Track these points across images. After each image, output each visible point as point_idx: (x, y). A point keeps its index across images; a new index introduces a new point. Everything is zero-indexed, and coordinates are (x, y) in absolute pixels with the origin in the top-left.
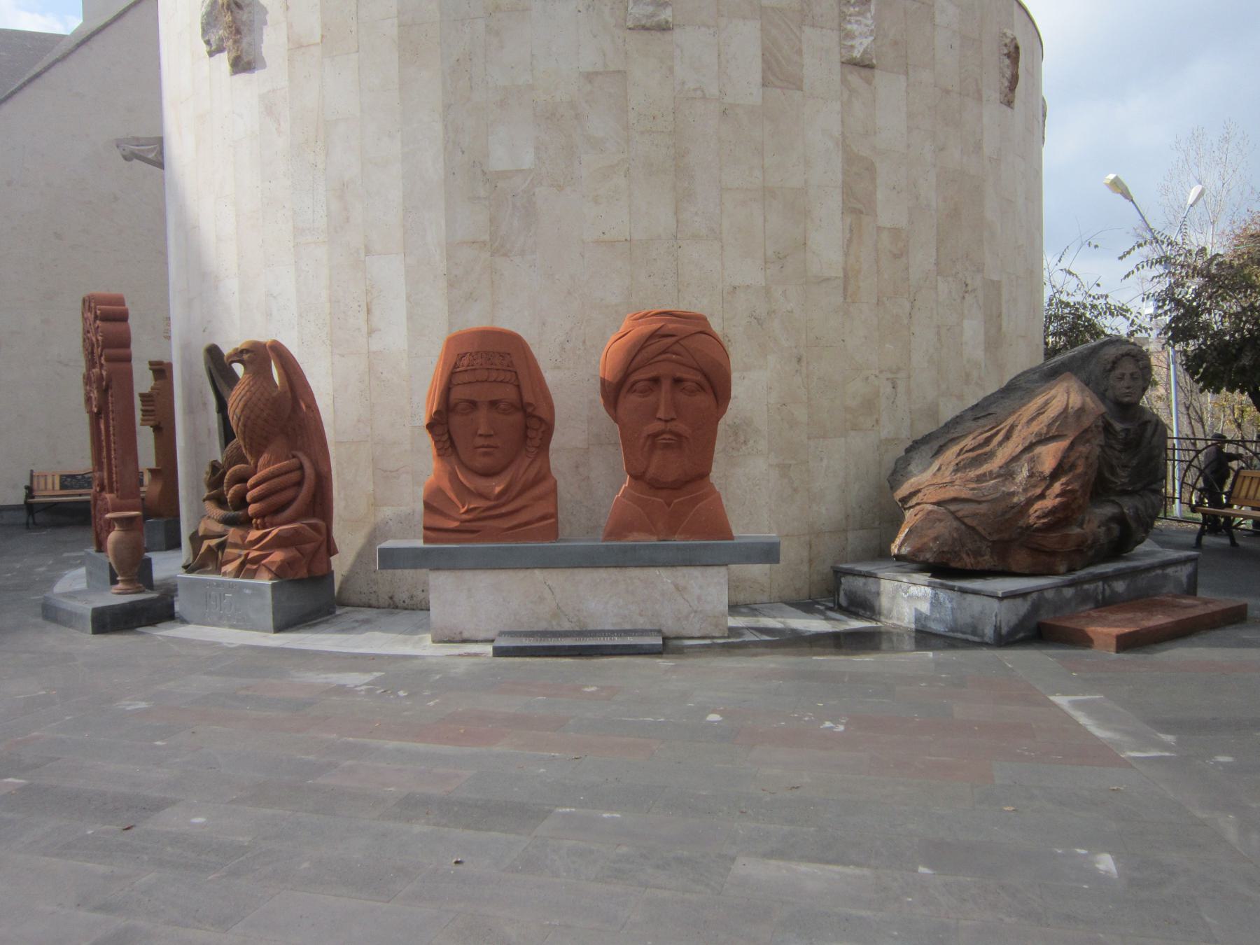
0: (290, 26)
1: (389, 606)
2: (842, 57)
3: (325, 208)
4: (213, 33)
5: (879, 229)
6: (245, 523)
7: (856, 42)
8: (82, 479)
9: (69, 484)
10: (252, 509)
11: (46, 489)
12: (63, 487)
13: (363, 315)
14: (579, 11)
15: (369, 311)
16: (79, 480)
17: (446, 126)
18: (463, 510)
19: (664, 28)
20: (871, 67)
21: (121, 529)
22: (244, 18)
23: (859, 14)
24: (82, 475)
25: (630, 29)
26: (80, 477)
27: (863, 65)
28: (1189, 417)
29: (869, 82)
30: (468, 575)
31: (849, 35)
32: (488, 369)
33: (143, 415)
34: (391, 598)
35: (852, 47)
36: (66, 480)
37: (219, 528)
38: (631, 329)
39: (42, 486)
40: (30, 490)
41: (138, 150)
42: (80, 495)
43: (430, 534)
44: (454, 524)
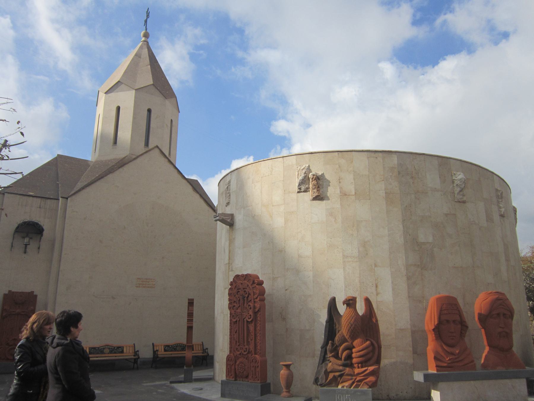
0: (341, 188)
1: (387, 399)
2: (499, 214)
3: (357, 249)
4: (303, 186)
6: (351, 366)
8: (98, 349)
9: (92, 352)
12: (165, 350)
13: (374, 288)
14: (442, 195)
15: (376, 287)
16: (170, 348)
17: (403, 226)
18: (447, 359)
19: (464, 202)
21: (287, 369)
22: (321, 183)
24: (98, 348)
25: (456, 202)
26: (97, 349)
31: (500, 208)
32: (452, 309)
34: (388, 396)
37: (341, 368)
38: (488, 297)
41: (225, 218)
42: (97, 357)
43: (438, 368)
44: (445, 365)
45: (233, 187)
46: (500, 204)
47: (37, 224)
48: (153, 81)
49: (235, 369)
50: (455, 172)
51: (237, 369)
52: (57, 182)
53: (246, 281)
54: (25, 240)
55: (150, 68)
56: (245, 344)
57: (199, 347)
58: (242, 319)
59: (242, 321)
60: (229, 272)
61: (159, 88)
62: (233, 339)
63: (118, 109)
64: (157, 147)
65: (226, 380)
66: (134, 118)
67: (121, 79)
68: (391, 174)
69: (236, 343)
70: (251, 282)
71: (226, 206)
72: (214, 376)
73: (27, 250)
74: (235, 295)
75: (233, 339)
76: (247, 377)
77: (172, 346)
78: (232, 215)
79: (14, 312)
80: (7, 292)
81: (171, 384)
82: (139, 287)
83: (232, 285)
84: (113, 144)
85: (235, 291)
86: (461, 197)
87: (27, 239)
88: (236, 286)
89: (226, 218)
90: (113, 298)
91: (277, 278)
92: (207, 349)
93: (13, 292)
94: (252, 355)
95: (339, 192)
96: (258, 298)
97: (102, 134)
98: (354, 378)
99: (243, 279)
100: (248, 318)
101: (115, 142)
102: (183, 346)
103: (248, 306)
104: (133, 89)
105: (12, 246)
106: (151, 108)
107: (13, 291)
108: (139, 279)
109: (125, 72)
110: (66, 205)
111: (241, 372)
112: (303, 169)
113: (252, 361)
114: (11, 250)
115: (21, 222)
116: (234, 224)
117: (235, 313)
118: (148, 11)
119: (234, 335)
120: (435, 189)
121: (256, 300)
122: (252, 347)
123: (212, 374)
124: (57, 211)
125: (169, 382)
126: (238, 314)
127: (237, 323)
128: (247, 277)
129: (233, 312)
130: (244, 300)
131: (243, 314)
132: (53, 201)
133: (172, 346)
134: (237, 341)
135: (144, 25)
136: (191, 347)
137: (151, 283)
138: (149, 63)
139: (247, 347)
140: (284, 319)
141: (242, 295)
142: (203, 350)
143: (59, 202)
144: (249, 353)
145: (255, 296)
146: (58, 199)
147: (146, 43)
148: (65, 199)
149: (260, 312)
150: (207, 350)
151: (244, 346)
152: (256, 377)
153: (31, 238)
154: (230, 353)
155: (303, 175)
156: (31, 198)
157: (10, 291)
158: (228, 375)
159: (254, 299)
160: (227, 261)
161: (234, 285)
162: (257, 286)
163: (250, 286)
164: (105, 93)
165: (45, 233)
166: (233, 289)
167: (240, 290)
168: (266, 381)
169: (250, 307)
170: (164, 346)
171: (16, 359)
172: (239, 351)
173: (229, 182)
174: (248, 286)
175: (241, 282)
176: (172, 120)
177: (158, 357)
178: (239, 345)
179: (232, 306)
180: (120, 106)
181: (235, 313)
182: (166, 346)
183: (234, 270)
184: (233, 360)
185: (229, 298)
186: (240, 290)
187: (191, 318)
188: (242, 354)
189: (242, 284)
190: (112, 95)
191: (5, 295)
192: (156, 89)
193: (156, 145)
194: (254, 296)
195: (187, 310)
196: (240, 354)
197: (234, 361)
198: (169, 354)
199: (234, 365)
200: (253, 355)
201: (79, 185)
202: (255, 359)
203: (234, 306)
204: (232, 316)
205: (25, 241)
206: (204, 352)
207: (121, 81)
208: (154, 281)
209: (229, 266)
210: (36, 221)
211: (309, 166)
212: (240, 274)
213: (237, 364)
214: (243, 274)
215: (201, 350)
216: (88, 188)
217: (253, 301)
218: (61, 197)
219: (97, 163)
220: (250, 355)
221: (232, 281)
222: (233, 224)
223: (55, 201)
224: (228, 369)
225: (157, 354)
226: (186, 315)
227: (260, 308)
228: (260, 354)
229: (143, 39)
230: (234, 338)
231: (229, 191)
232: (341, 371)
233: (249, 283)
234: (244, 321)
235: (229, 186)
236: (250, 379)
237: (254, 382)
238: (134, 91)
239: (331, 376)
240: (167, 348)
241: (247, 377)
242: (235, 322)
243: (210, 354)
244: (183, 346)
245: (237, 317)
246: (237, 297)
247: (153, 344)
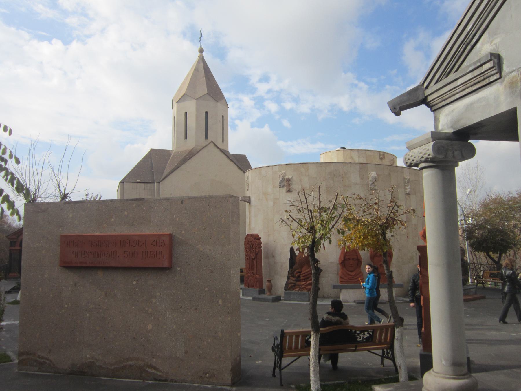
1: (323, 298)
5: (412, 224)
7: (407, 190)
10: (301, 278)
20: (410, 194)
22: (291, 182)
23: (407, 185)
27: (408, 194)
28: (472, 254)
29: (409, 197)
30: (349, 290)
31: (406, 189)
35: (407, 191)
44: (346, 281)
46: (406, 187)
50: (370, 172)
52: (153, 170)
53: (251, 238)
55: (205, 80)
61: (212, 95)
63: (186, 113)
64: (212, 142)
68: (330, 176)
76: (253, 286)
78: (249, 197)
85: (247, 243)
86: (373, 187)
95: (300, 188)
98: (300, 286)
104: (194, 99)
106: (207, 111)
109: (189, 86)
112: (281, 174)
120: (356, 183)
121: (256, 248)
122: (255, 271)
124: (154, 190)
128: (252, 235)
132: (151, 184)
138: (204, 75)
140: (273, 257)
144: (254, 274)
146: (154, 183)
147: (201, 57)
148: (158, 183)
155: (282, 178)
156: (139, 184)
159: (255, 247)
162: (257, 241)
163: (253, 240)
168: (263, 288)
171: (327, 318)
174: (252, 240)
179: (246, 250)
193: (211, 141)
201: (166, 172)
207: (186, 94)
211: (285, 172)
213: (249, 279)
216: (171, 175)
217: (255, 248)
218: (156, 182)
220: (254, 275)
232: (294, 283)
239: (290, 286)
241: (253, 286)
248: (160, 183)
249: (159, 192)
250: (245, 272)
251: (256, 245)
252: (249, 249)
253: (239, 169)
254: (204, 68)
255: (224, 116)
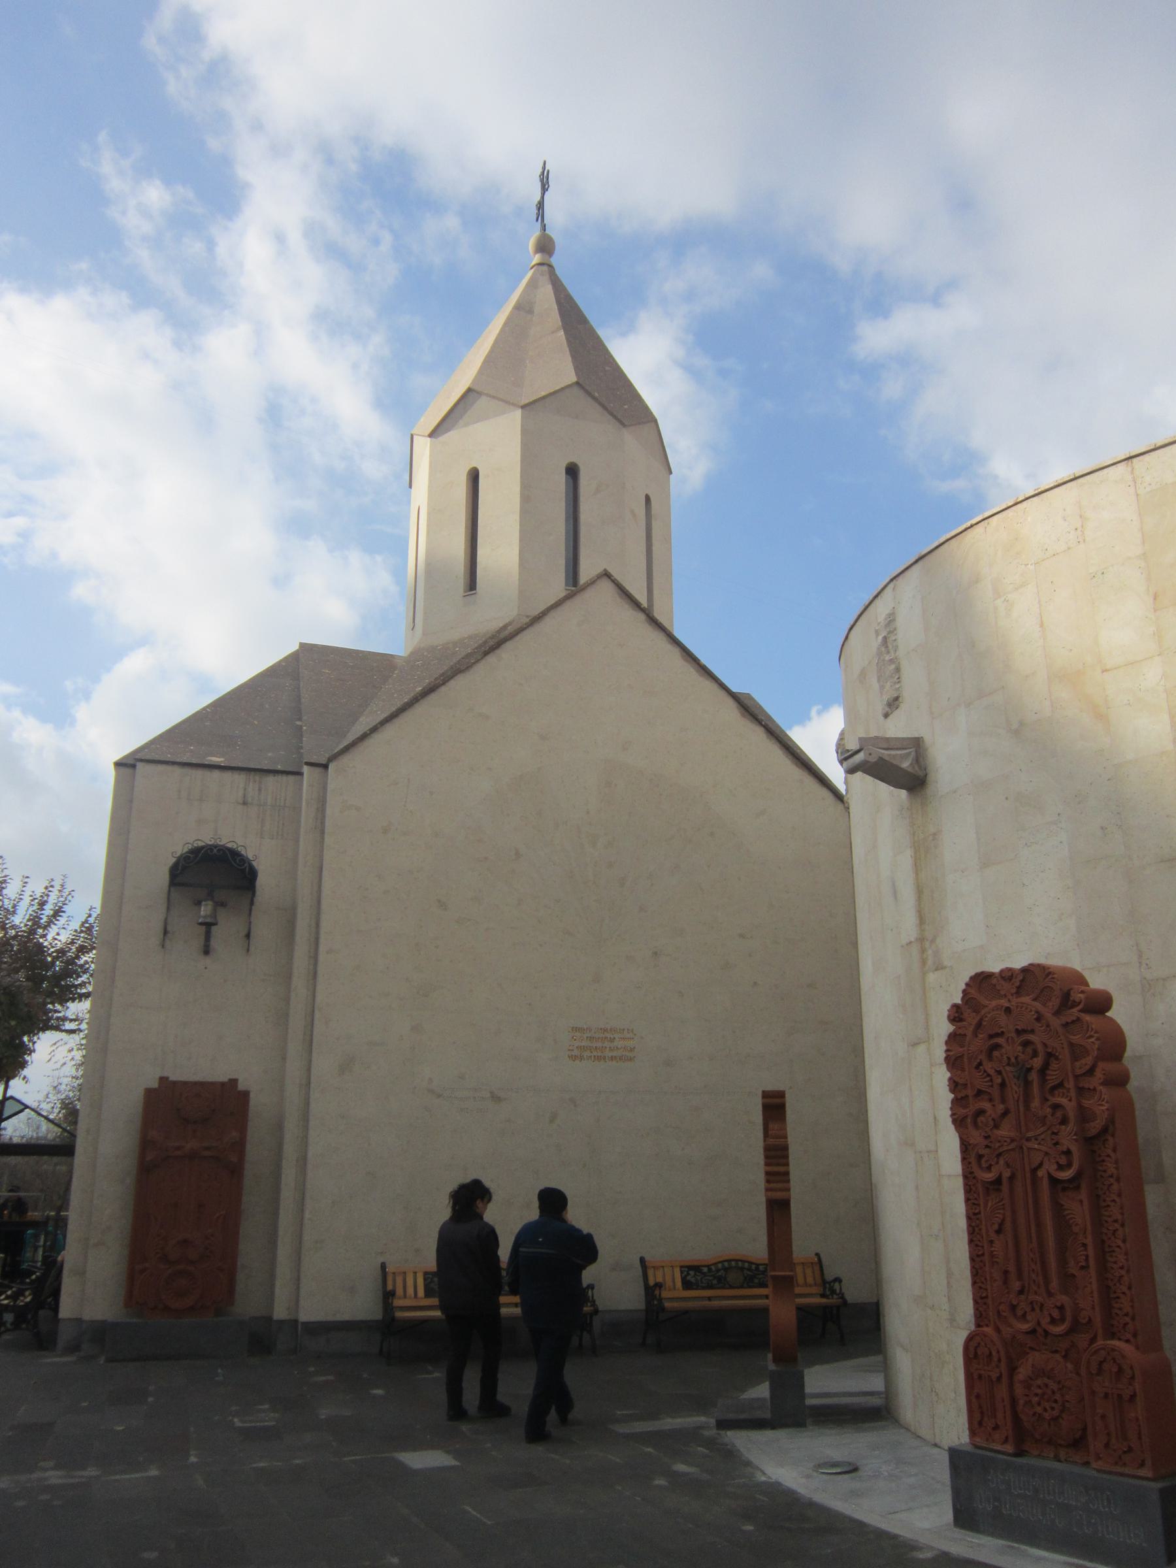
11: (405, 1296)
12: (687, 1285)
16: (704, 1274)
33: (768, 1181)
36: (688, 1274)
39: (399, 1291)
40: (388, 1296)
41: (890, 755)
45: (910, 632)
47: (235, 854)
48: (577, 374)
49: (1013, 1401)
51: (1021, 1402)
52: (298, 723)
53: (1026, 999)
54: (202, 908)
55: (564, 337)
56: (1054, 1284)
57: (809, 1272)
58: (1028, 1175)
59: (1028, 1182)
60: (924, 974)
61: (596, 394)
62: (986, 1258)
63: (474, 477)
64: (606, 575)
65: (970, 1448)
66: (525, 498)
67: (474, 381)
69: (1005, 1282)
70: (1055, 1002)
71: (886, 716)
72: (889, 1393)
73: (214, 943)
74: (980, 1064)
75: (986, 1258)
76: (1078, 1443)
77: (710, 1270)
78: (917, 745)
79: (178, 1148)
80: (155, 1085)
81: (723, 1432)
82: (581, 1058)
83: (961, 1020)
84: (465, 592)
87: (206, 905)
88: (979, 1025)
89: (894, 756)
90: (496, 1099)
91: (1164, 980)
92: (838, 1280)
93: (174, 1083)
94: (1093, 1340)
96: (1099, 1073)
97: (428, 564)
99: (1014, 991)
100: (1055, 1166)
101: (472, 584)
102: (749, 1269)
103: (1049, 1110)
104: (514, 405)
105: (166, 932)
107: (173, 1078)
108: (575, 1029)
110: (324, 788)
111: (1047, 1415)
113: (1100, 1371)
114: (163, 946)
115: (186, 850)
116: (931, 778)
117: (986, 1142)
118: (544, 172)
119: (991, 1242)
123: (876, 1383)
125: (712, 1421)
126: (1005, 1148)
127: (999, 1190)
129: (976, 1137)
130: (1027, 1084)
131: (1029, 1149)
132: (284, 779)
133: (708, 1266)
134: (1012, 1268)
135: (535, 220)
136: (785, 1284)
137: (621, 1042)
138: (561, 324)
139: (1064, 1299)
141: (1013, 1060)
142: (824, 1282)
143: (301, 785)
145: (1083, 1061)
147: (545, 268)
148: (318, 770)
149: (1113, 1136)
150: (837, 1286)
151: (1050, 1294)
152: (1130, 1450)
153: (223, 904)
154: (978, 1325)
156: (216, 774)
157: (163, 1080)
158: (980, 1424)
159: (1076, 1077)
160: (909, 927)
161: (971, 1019)
162: (1087, 1018)
163: (1048, 1015)
164: (431, 435)
165: (261, 881)
166: (968, 1039)
167: (1000, 1040)
169: (1059, 1114)
170: (681, 1267)
172: (1024, 1315)
173: (891, 619)
175: (1004, 1003)
176: (648, 499)
177: (663, 1309)
178: (1021, 1292)
180: (478, 467)
181: (986, 1142)
182: (690, 1268)
183: (946, 963)
184: (999, 1360)
185: (950, 1079)
186: (1000, 1040)
187: (782, 1169)
188: (1039, 1330)
189: (1008, 1010)
190: (452, 437)
191: (149, 1092)
192: (589, 399)
194: (1078, 1064)
195: (761, 1135)
196: (1033, 1332)
197: (1003, 1365)
198: (702, 1298)
199: (1005, 1379)
200: (1100, 1342)
202: (1114, 1359)
203: (981, 1112)
204: (973, 1160)
205: (202, 913)
206: (828, 1293)
207: (476, 388)
208: (631, 1035)
209: (923, 951)
210: (230, 845)
212: (996, 968)
214: (1009, 969)
215: (816, 1284)
217: (1070, 1084)
219: (418, 657)
221: (958, 1001)
222: (926, 775)
223: (291, 778)
224: (978, 1396)
225: (660, 1300)
226: (759, 1157)
227: (1111, 1120)
228: (1135, 1335)
229: (537, 258)
230: (992, 1256)
231: (892, 652)
233: (1044, 1005)
234: (1035, 1181)
235: (890, 632)
236: (1098, 1458)
237: (1119, 1469)
238: (518, 413)
240: (694, 1275)
242: (992, 1183)
243: (854, 1293)
244: (749, 1269)
245: (1002, 1162)
246: (991, 1072)
247: (642, 1260)
248: (332, 767)
249: (324, 817)
250: (806, 1284)
251: (1088, 1061)
252: (1003, 1100)
253: (743, 715)
254: (558, 302)
255: (652, 499)
